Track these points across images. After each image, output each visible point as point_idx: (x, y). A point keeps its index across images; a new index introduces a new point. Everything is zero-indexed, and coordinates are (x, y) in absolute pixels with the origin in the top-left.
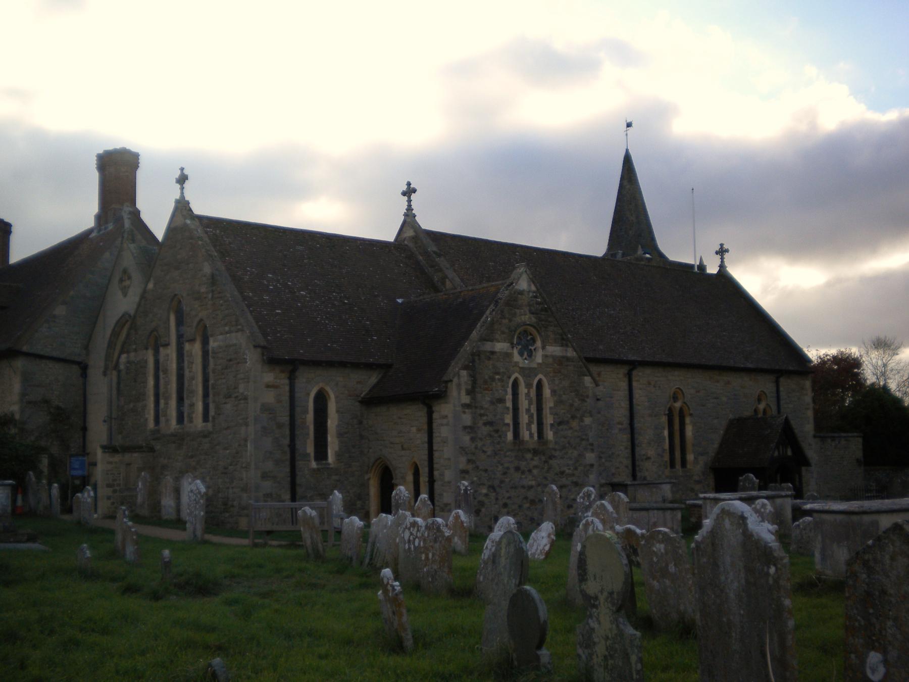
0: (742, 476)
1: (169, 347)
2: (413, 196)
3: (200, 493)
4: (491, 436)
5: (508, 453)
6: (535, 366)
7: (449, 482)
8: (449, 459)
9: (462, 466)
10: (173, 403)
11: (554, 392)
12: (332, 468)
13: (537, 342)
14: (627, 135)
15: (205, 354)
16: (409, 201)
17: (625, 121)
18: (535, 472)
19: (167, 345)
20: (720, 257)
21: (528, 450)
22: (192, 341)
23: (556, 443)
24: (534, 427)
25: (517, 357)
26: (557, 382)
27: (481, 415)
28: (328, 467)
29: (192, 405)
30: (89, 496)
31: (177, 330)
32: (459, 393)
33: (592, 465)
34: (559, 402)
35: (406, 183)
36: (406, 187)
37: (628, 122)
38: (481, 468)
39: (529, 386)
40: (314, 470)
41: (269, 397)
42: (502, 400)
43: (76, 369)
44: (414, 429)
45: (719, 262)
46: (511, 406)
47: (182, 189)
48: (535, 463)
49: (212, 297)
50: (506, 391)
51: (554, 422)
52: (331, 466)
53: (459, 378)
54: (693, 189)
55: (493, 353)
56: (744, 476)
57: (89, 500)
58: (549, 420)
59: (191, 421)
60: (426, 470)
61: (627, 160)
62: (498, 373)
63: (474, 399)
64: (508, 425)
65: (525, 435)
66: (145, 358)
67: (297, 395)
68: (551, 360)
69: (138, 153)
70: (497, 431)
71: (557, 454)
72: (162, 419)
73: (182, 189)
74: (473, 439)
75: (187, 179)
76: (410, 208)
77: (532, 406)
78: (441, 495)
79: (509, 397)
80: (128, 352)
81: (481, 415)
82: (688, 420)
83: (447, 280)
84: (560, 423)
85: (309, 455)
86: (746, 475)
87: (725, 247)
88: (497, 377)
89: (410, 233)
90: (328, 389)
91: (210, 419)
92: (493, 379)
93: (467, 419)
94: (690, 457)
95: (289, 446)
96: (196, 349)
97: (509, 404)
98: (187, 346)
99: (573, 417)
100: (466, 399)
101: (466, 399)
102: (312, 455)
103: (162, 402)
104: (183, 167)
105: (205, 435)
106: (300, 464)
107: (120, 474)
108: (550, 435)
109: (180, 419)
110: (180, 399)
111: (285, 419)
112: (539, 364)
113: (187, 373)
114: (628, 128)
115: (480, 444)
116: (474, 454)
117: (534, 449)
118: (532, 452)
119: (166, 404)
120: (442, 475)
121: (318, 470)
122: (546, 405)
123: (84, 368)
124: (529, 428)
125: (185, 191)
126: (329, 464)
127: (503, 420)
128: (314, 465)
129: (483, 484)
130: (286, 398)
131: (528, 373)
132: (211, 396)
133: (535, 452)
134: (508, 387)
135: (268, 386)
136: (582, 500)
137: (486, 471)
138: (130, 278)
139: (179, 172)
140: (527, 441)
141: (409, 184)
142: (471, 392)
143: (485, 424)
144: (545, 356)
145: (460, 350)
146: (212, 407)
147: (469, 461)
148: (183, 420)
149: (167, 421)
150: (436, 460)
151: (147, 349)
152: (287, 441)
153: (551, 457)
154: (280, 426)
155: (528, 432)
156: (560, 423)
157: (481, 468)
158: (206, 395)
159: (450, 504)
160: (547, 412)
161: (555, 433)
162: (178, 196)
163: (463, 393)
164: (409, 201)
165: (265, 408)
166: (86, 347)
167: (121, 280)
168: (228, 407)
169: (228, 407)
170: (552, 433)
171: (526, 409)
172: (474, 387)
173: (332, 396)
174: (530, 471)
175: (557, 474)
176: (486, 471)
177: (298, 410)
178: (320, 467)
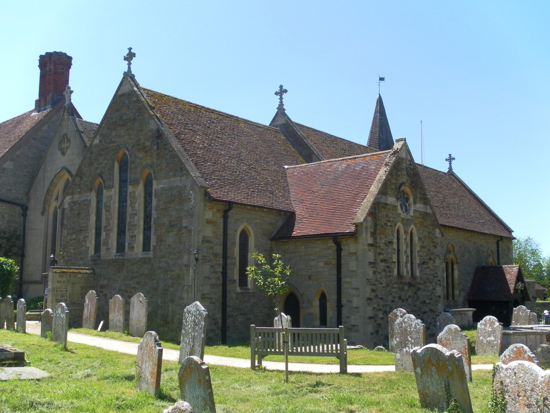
0: (516, 307)
1: (113, 189)
2: (284, 96)
3: (200, 314)
4: (385, 271)
5: (395, 286)
6: (409, 218)
7: (357, 308)
8: (357, 289)
9: (368, 295)
10: (114, 235)
11: (420, 239)
12: (251, 293)
13: (410, 200)
14: (379, 85)
15: (148, 195)
16: (281, 99)
17: (378, 76)
18: (410, 300)
19: (111, 187)
20: (449, 163)
21: (406, 283)
22: (135, 183)
23: (421, 278)
24: (409, 265)
25: (399, 210)
26: (421, 232)
27: (380, 254)
28: (248, 291)
29: (133, 236)
30: (63, 312)
31: (120, 177)
32: (367, 235)
33: (440, 297)
34: (422, 247)
35: (279, 86)
36: (279, 88)
37: (380, 77)
38: (379, 296)
39: (406, 232)
40: (238, 294)
41: (208, 232)
42: (391, 243)
43: (18, 209)
44: (322, 264)
45: (448, 166)
46: (396, 248)
47: (129, 64)
48: (410, 293)
49: (158, 148)
50: (394, 237)
51: (420, 262)
52: (250, 291)
53: (367, 223)
54: (421, 121)
55: (386, 204)
56: (518, 308)
57: (63, 316)
58: (417, 261)
59: (132, 248)
60: (335, 297)
61: (380, 102)
62: (389, 221)
63: (375, 239)
64: (395, 262)
65: (404, 272)
66: (89, 199)
67: (229, 232)
68: (418, 215)
69: (72, 57)
70: (388, 267)
71: (422, 287)
72: (103, 248)
73: (129, 64)
74: (374, 273)
75: (135, 57)
76: (281, 104)
77: (408, 249)
78: (348, 317)
79: (395, 241)
80: (72, 194)
81: (380, 254)
82: (455, 267)
83: (313, 156)
84: (423, 263)
85: (235, 281)
86: (520, 306)
87: (453, 156)
88: (389, 224)
89: (281, 121)
90: (250, 228)
91: (152, 248)
92: (386, 224)
93: (371, 257)
94: (457, 292)
95: (222, 273)
96: (140, 190)
97: (395, 246)
98: (130, 189)
99: (430, 259)
100: (370, 241)
101: (370, 241)
102: (238, 281)
103: (103, 234)
104: (131, 47)
105: (145, 261)
106: (229, 287)
107: (67, 291)
108: (418, 273)
109: (121, 248)
110: (121, 232)
111: (219, 249)
112: (412, 216)
113: (129, 211)
114: (380, 81)
115: (379, 276)
116: (375, 285)
117: (409, 283)
118: (408, 285)
119: (108, 235)
120: (350, 301)
121: (242, 293)
122: (416, 249)
123: (25, 209)
124: (406, 267)
125: (131, 66)
126: (248, 289)
127: (391, 258)
128: (238, 290)
129: (380, 310)
130: (220, 232)
131: (406, 223)
132: (153, 229)
133: (410, 285)
134: (395, 233)
135: (208, 222)
136: (483, 327)
137: (382, 299)
138: (69, 140)
139: (128, 51)
140: (405, 276)
141: (281, 87)
142: (373, 234)
143: (382, 261)
144: (415, 211)
145: (360, 202)
146: (153, 239)
147: (373, 291)
148: (124, 249)
149: (108, 249)
150: (343, 290)
151: (91, 190)
152: (220, 269)
153: (419, 289)
154: (216, 255)
155: (406, 269)
156: (423, 263)
157: (379, 296)
158: (147, 228)
159: (358, 326)
160: (416, 254)
161: (421, 271)
162: (126, 70)
163: (369, 235)
164: (281, 99)
165: (205, 240)
166: (27, 194)
167: (60, 143)
168: (170, 239)
169: (170, 239)
170: (418, 270)
171: (405, 251)
172: (375, 230)
173: (252, 234)
174: (407, 300)
175: (421, 303)
176: (382, 299)
177: (229, 243)
178: (243, 291)
